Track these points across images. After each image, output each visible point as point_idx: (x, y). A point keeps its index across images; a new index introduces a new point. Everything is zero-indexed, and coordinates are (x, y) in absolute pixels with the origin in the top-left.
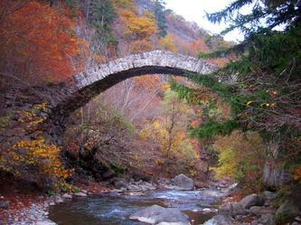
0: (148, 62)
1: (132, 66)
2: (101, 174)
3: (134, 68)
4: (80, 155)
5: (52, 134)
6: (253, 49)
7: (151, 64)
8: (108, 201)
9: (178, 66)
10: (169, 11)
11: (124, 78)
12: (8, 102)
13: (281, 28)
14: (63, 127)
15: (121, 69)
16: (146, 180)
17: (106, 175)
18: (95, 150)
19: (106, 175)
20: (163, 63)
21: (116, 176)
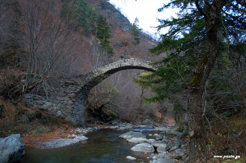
0: (127, 64)
1: (120, 66)
2: (105, 119)
3: (121, 67)
4: (95, 110)
5: (82, 99)
6: (74, 60)
7: (129, 65)
8: (95, 135)
9: (142, 66)
10: (140, 30)
11: (152, 71)
12: (61, 84)
13: (180, 35)
14: (87, 95)
15: (115, 67)
16: (128, 122)
17: (108, 119)
18: (103, 106)
19: (108, 119)
20: (135, 64)
21: (113, 120)
